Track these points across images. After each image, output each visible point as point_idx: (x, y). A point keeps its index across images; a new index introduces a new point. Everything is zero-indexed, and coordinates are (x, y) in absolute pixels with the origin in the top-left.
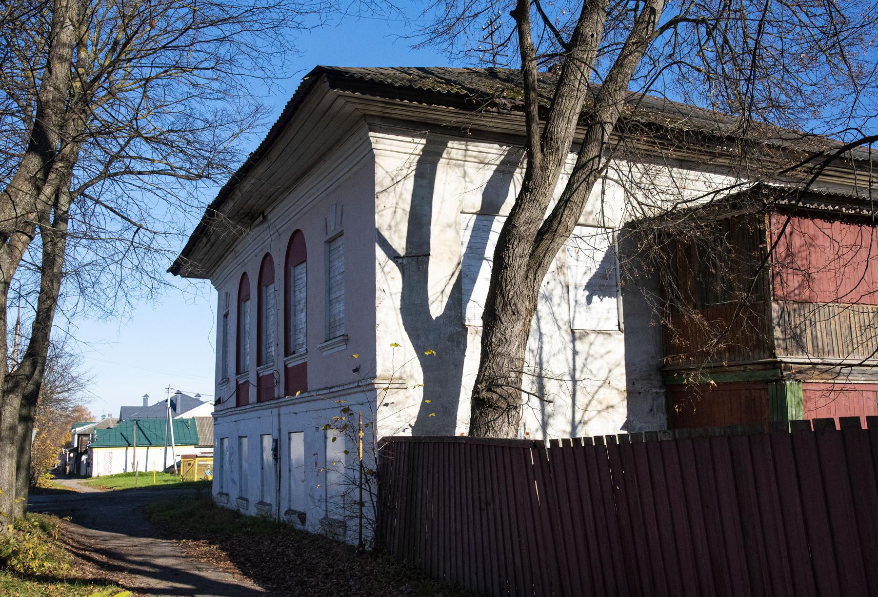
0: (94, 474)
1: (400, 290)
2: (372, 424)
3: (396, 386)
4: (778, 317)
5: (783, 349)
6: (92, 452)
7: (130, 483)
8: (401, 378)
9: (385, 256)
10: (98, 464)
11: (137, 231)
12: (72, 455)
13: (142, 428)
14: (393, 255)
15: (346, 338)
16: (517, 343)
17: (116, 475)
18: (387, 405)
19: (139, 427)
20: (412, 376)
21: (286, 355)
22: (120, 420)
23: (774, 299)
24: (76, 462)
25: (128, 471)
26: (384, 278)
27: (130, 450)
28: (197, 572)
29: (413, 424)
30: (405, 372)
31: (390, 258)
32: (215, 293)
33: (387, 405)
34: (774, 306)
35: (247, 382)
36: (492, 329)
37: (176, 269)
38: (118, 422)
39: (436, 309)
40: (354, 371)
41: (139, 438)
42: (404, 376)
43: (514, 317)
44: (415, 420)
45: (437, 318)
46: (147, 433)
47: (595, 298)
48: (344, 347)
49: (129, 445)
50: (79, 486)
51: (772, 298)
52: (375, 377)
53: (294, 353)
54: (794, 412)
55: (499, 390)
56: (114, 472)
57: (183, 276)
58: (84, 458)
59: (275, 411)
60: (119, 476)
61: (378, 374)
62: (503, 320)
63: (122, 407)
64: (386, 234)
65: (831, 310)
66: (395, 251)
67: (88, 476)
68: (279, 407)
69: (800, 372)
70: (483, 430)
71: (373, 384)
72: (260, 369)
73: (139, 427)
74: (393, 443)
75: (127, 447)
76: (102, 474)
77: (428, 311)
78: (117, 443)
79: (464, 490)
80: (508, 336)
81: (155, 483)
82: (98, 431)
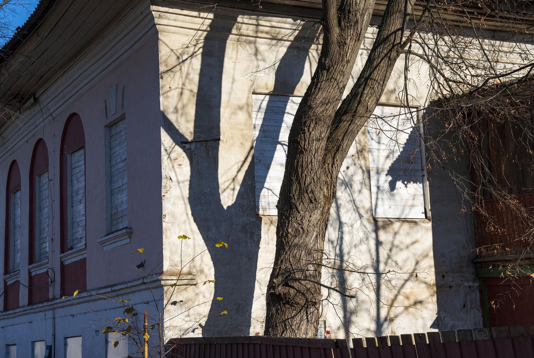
9: (172, 141)
16: (315, 234)
18: (174, 303)
20: (202, 271)
21: (62, 251)
26: (171, 165)
29: (203, 324)
30: (195, 266)
33: (174, 303)
36: (287, 218)
42: (194, 271)
43: (311, 206)
45: (228, 207)
47: (399, 184)
48: (128, 241)
52: (162, 273)
53: (72, 248)
55: (296, 285)
59: (49, 314)
61: (165, 268)
62: (300, 208)
64: (172, 117)
66: (182, 136)
68: (54, 309)
72: (33, 268)
80: (305, 226)
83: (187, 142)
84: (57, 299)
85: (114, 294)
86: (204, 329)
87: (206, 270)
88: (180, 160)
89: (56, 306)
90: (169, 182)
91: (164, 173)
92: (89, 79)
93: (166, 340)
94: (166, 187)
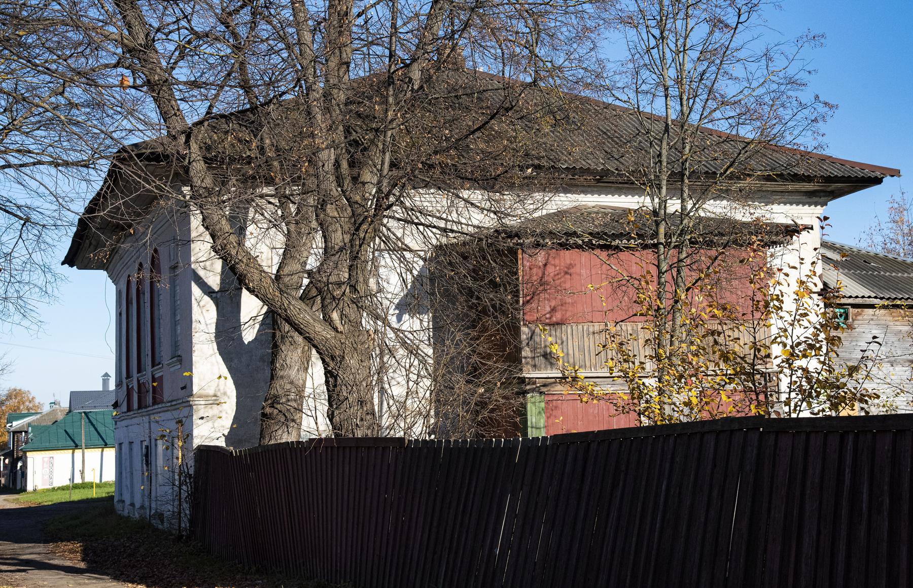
0: (30, 488)
1: (215, 320)
2: (189, 436)
3: (211, 402)
4: (527, 339)
5: (531, 365)
6: (26, 457)
7: (77, 496)
8: (215, 396)
9: (201, 292)
10: (34, 473)
11: (24, 224)
12: (7, 461)
13: (94, 422)
14: (207, 290)
15: (179, 358)
16: (296, 368)
17: (59, 488)
18: (202, 418)
19: (90, 421)
20: (225, 394)
21: (153, 366)
22: (70, 411)
23: (524, 324)
24: (11, 471)
25: (76, 482)
26: (200, 311)
27: (78, 453)
28: (47, 561)
29: (226, 434)
30: (219, 390)
31: (205, 294)
32: (112, 288)
33: (202, 418)
34: (524, 329)
35: (133, 387)
36: (276, 356)
37: (71, 260)
38: (68, 414)
39: (249, 335)
40: (183, 388)
41: (88, 434)
42: (219, 394)
43: (292, 347)
44: (228, 430)
45: (249, 342)
46: (101, 429)
47: (406, 317)
48: (179, 366)
49: (77, 446)
50: (5, 503)
51: (522, 323)
52: (192, 395)
53: (159, 364)
54: (534, 420)
55: (278, 406)
56: (57, 484)
57: (79, 268)
58: (20, 464)
59: (146, 419)
60: (63, 489)
61: (195, 392)
62: (283, 349)
63: (72, 394)
64: (201, 273)
65: (585, 329)
66: (209, 287)
67: (23, 490)
68: (149, 415)
69: (545, 385)
70: (267, 439)
71: (189, 401)
72: (142, 376)
73: (90, 421)
74: (206, 453)
75: (103, 448)
76: (40, 487)
77: (242, 338)
78: (60, 444)
79: (346, 493)
80: (288, 362)
81: (95, 496)
82: (34, 427)
83: (214, 292)
84: (149, 406)
85: (174, 407)
86: (228, 438)
87: (229, 393)
88: (208, 307)
89: (151, 412)
90: (198, 325)
91: (194, 317)
92: (162, 224)
93: (195, 445)
94: (195, 328)
